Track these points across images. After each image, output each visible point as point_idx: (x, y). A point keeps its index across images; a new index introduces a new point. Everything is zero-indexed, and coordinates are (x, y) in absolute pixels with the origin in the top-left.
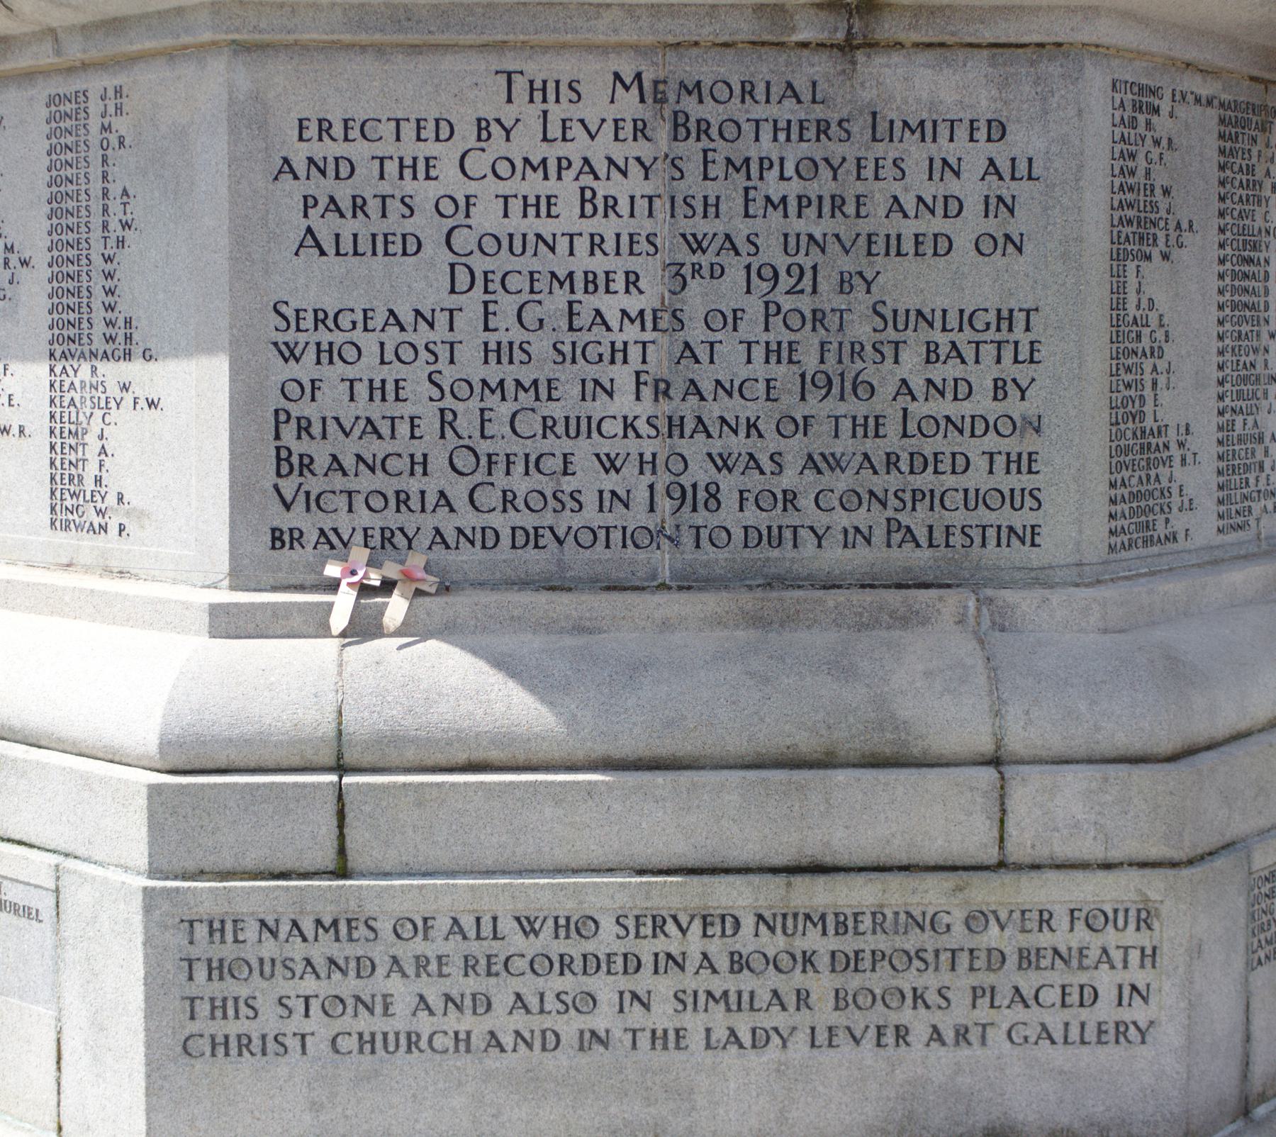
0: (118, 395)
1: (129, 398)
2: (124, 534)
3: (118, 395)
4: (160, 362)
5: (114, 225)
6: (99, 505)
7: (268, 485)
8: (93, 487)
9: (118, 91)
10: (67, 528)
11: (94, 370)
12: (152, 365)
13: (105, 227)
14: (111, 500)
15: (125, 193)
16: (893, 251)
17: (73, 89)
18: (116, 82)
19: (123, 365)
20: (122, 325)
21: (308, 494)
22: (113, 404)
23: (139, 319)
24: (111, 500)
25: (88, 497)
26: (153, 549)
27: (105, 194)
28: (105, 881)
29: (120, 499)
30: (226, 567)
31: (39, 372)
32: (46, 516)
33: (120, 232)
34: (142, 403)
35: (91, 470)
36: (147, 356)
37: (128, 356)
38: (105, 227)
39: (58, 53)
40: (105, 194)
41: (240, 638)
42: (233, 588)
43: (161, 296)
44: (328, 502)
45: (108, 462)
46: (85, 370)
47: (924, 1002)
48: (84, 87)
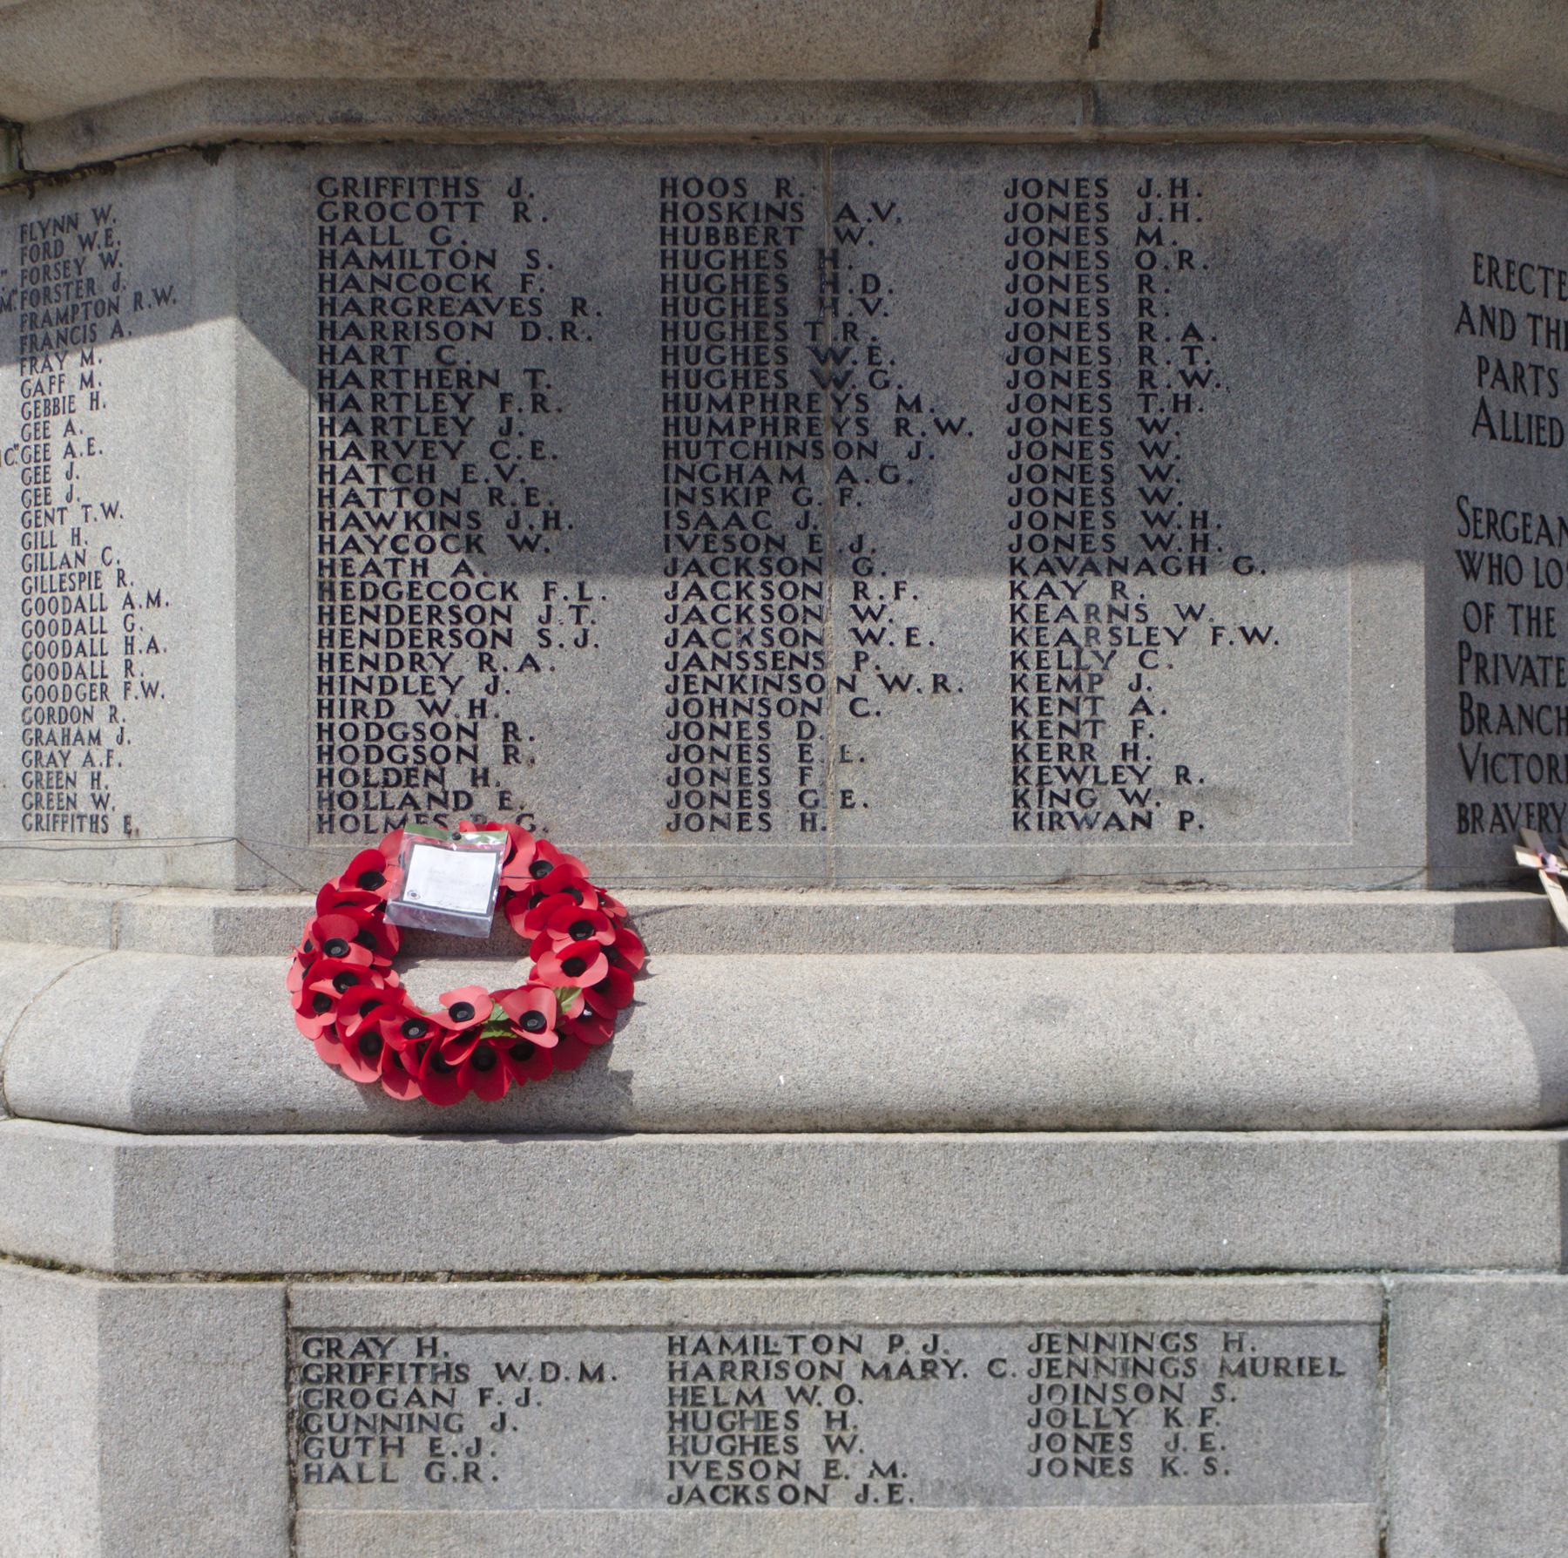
0: (1176, 624)
1: (1202, 630)
2: (1189, 826)
3: (1176, 624)
4: (1272, 576)
5: (1166, 376)
6: (1132, 785)
7: (1454, 743)
8: (1117, 760)
9: (1180, 187)
10: (1056, 823)
11: (1118, 590)
12: (1255, 582)
13: (1146, 378)
14: (1162, 776)
15: (1192, 331)
16: (1534, 441)
17: (1073, 175)
18: (1177, 172)
19: (1185, 580)
20: (1187, 522)
21: (1485, 756)
22: (1163, 637)
23: (1223, 514)
24: (1162, 776)
25: (1106, 774)
26: (1261, 844)
27: (1146, 331)
28: (1471, 1289)
29: (1182, 774)
30: (1422, 858)
31: (995, 591)
32: (1003, 809)
33: (1179, 387)
34: (1231, 633)
35: (1115, 733)
36: (1242, 565)
37: (1199, 566)
38: (1146, 378)
39: (1099, 120)
40: (1146, 331)
41: (1483, 950)
42: (1431, 887)
43: (1275, 482)
44: (1506, 769)
45: (1150, 724)
46: (1097, 590)
47: (1172, 1470)
48: (1100, 173)
